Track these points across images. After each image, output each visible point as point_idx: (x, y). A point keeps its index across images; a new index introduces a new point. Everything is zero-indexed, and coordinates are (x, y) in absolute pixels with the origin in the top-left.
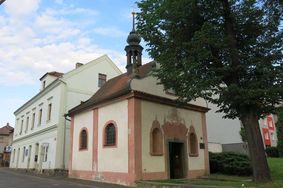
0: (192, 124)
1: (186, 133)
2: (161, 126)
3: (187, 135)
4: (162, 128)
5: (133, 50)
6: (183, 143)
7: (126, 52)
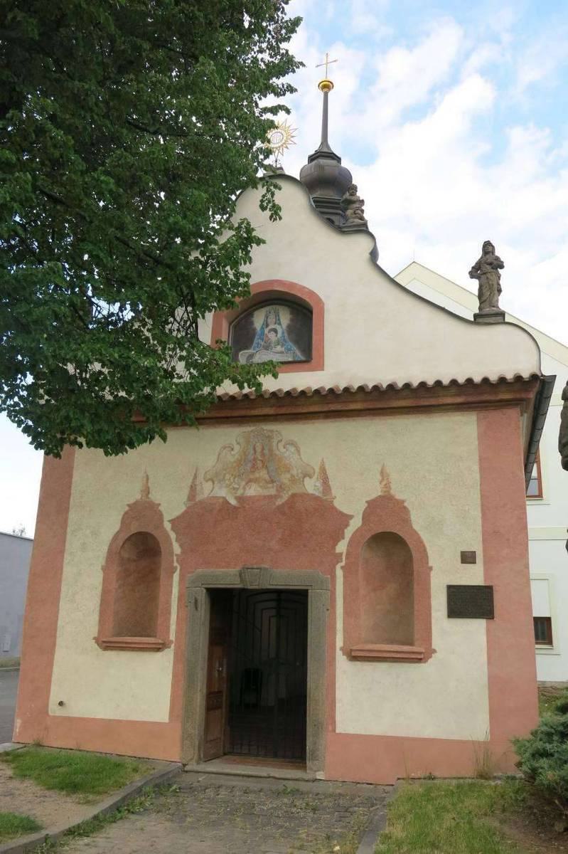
1: (338, 536)
2: (169, 521)
3: (342, 547)
6: (307, 591)
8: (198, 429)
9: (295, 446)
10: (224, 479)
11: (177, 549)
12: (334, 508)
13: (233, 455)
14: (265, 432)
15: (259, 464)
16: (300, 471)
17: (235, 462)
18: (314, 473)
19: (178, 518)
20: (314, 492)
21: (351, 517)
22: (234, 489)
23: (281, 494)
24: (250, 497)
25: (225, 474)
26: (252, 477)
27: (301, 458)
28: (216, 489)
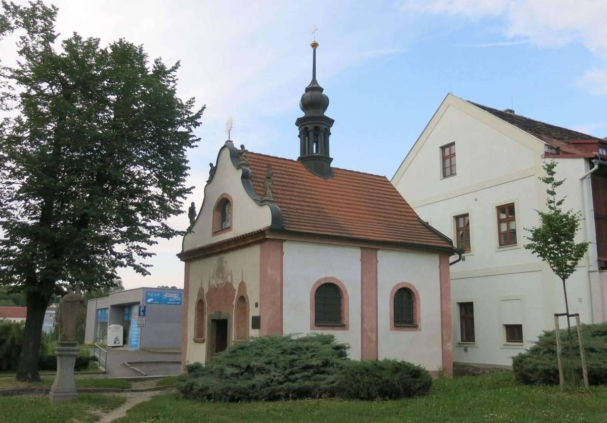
0: (243, 280)
5: (310, 127)
7: (299, 129)
11: (207, 305)
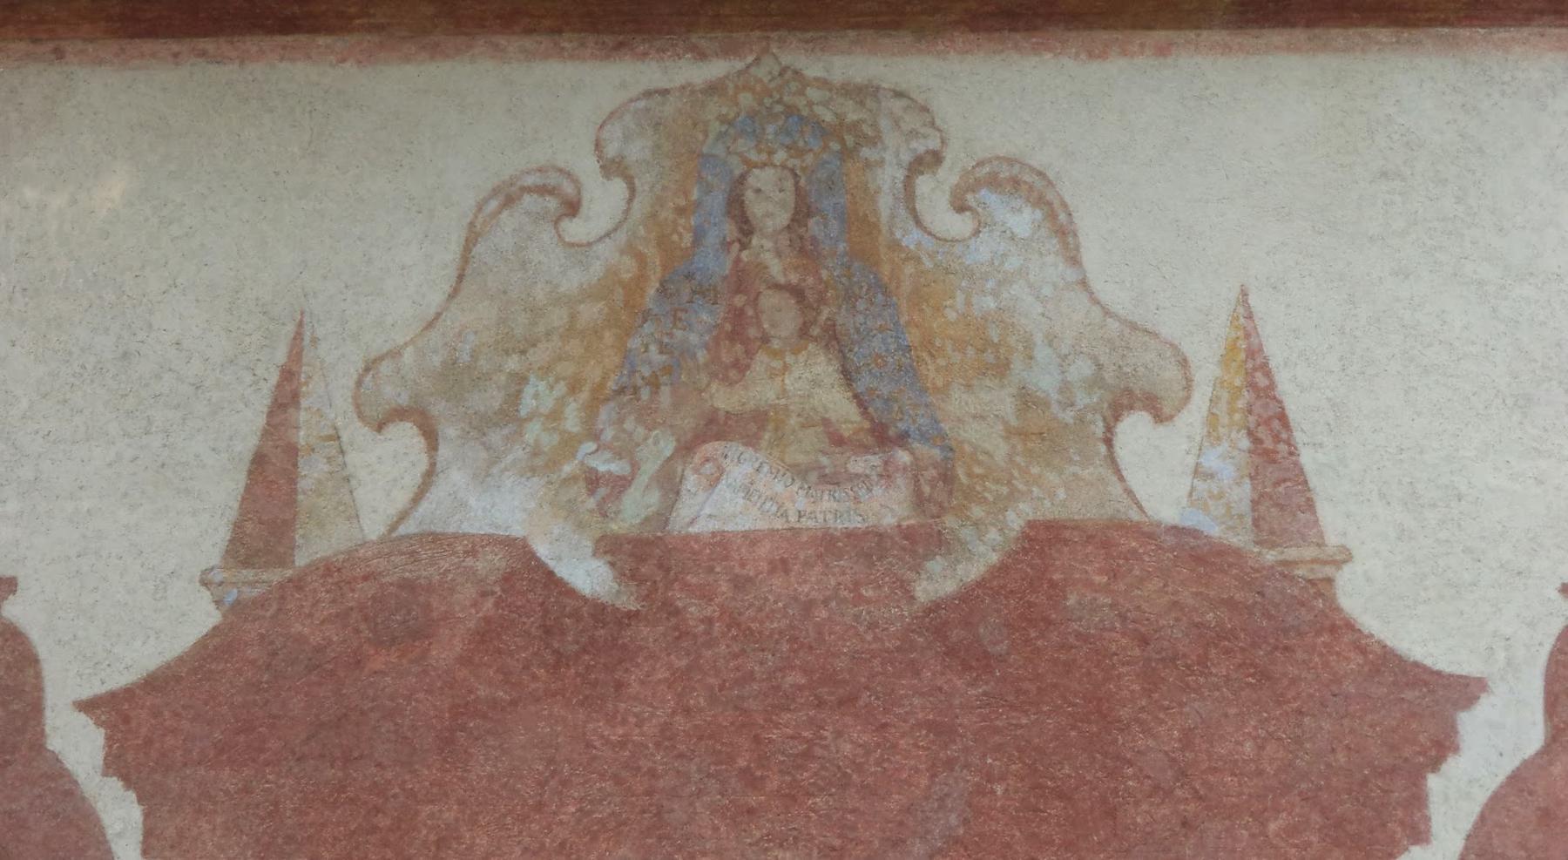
2: (87, 706)
4: (117, 764)
8: (644, 62)
9: (1040, 201)
10: (509, 415)
12: (1340, 627)
13: (580, 249)
14: (813, 94)
15: (781, 316)
16: (1081, 369)
17: (589, 294)
18: (1188, 385)
19: (154, 683)
20: (1194, 519)
21: (1467, 690)
22: (593, 481)
23: (950, 521)
24: (721, 544)
25: (520, 379)
26: (723, 399)
27: (1084, 283)
28: (455, 478)
